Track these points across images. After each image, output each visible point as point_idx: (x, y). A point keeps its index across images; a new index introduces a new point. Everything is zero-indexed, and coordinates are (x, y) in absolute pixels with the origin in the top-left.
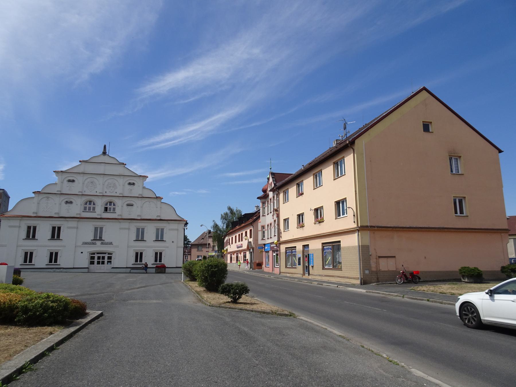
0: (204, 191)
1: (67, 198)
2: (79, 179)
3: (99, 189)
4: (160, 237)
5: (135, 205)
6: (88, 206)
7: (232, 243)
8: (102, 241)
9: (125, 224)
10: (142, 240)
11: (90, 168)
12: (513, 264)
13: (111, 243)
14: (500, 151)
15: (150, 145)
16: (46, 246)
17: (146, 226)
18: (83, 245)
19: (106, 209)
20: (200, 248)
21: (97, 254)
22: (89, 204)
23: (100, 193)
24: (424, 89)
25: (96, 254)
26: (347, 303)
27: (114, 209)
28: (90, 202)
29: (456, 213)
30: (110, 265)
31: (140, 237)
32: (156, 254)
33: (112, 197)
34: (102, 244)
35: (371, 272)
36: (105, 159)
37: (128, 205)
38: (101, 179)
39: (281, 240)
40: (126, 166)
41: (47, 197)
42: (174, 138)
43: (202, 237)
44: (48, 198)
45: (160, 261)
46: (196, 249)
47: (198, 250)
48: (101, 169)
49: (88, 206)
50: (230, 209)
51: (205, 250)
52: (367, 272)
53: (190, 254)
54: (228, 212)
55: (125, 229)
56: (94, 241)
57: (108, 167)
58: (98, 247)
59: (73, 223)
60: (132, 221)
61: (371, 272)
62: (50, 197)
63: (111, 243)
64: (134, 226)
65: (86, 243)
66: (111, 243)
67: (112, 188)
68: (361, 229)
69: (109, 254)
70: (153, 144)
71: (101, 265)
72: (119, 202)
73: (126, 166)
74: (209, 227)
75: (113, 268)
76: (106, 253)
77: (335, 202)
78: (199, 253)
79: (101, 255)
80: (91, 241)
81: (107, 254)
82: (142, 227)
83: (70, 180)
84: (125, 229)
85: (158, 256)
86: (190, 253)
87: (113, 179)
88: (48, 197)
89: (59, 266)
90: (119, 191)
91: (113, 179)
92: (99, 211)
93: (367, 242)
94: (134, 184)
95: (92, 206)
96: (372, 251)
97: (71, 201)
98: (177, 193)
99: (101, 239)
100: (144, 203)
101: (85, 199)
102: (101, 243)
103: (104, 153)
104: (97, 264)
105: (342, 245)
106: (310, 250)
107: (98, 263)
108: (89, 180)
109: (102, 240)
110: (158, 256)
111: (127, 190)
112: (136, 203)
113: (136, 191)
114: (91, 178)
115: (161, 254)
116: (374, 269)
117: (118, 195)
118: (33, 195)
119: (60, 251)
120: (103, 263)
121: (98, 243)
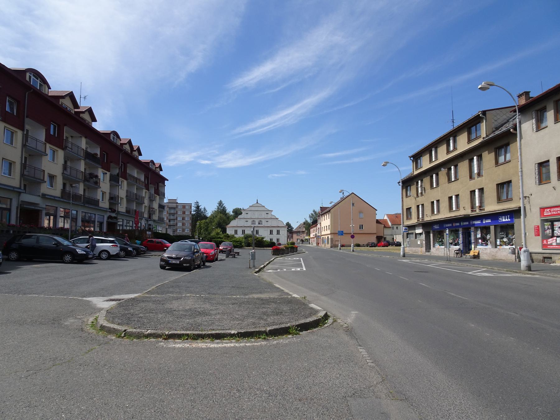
0: (303, 172)
2: (249, 213)
3: (256, 216)
4: (278, 232)
5: (269, 222)
6: (253, 222)
7: (327, 230)
9: (266, 229)
11: (253, 209)
12: (128, 235)
14: (376, 210)
15: (247, 131)
16: (275, 237)
19: (259, 223)
20: (298, 234)
22: (253, 222)
24: (353, 193)
26: (422, 283)
27: (262, 223)
28: (254, 221)
29: (360, 228)
31: (271, 232)
32: (277, 239)
35: (333, 245)
36: (257, 205)
37: (266, 222)
38: (257, 212)
39: (322, 234)
42: (269, 124)
43: (299, 227)
44: (240, 220)
45: (279, 242)
46: (296, 235)
47: (297, 235)
48: (256, 209)
49: (253, 222)
50: (314, 211)
51: (302, 236)
52: (332, 245)
53: (293, 238)
54: (313, 213)
55: (266, 230)
57: (259, 208)
61: (333, 245)
68: (331, 234)
70: (249, 131)
72: (263, 221)
74: (303, 221)
78: (298, 237)
84: (266, 230)
85: (278, 240)
86: (292, 237)
90: (263, 217)
92: (257, 224)
93: (332, 237)
94: (268, 214)
95: (254, 222)
96: (334, 239)
98: (276, 175)
103: (257, 203)
110: (278, 240)
111: (266, 216)
113: (269, 216)
115: (279, 239)
116: (334, 244)
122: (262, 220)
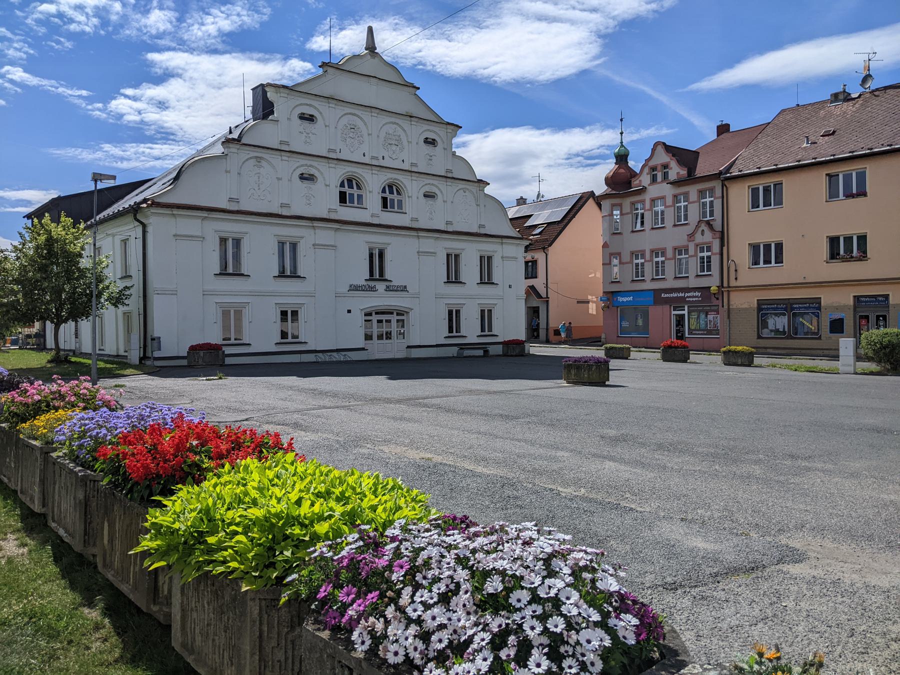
1: (302, 166)
2: (325, 112)
8: (388, 284)
9: (428, 243)
10: (457, 282)
13: (404, 289)
16: (273, 294)
17: (302, 237)
18: (351, 292)
21: (377, 313)
23: (373, 158)
25: (374, 314)
30: (403, 341)
32: (482, 311)
33: (401, 172)
34: (388, 289)
40: (418, 92)
41: (256, 157)
56: (372, 284)
58: (381, 299)
59: (325, 235)
60: (210, 216)
62: (267, 161)
63: (405, 287)
64: (823, 172)
65: (354, 288)
66: (405, 287)
67: (394, 148)
69: (398, 314)
71: (385, 341)
72: (413, 188)
73: (418, 92)
75: (408, 347)
76: (392, 313)
77: (827, 237)
79: (384, 317)
80: (365, 283)
81: (395, 314)
82: (291, 240)
83: (304, 114)
87: (395, 123)
88: (260, 158)
89: (464, 339)
91: (395, 123)
92: (371, 210)
94: (311, 119)
97: (313, 175)
99: (382, 278)
100: (245, 162)
101: (344, 171)
102: (385, 288)
104: (841, 321)
105: (892, 300)
106: (895, 306)
107: (380, 337)
108: (345, 120)
109: (386, 280)
112: (322, 173)
114: (349, 116)
117: (407, 169)
118: (321, 71)
119: (247, 308)
120: (389, 336)
121: (381, 286)
122: (405, 181)
